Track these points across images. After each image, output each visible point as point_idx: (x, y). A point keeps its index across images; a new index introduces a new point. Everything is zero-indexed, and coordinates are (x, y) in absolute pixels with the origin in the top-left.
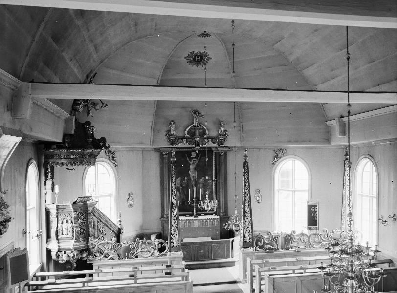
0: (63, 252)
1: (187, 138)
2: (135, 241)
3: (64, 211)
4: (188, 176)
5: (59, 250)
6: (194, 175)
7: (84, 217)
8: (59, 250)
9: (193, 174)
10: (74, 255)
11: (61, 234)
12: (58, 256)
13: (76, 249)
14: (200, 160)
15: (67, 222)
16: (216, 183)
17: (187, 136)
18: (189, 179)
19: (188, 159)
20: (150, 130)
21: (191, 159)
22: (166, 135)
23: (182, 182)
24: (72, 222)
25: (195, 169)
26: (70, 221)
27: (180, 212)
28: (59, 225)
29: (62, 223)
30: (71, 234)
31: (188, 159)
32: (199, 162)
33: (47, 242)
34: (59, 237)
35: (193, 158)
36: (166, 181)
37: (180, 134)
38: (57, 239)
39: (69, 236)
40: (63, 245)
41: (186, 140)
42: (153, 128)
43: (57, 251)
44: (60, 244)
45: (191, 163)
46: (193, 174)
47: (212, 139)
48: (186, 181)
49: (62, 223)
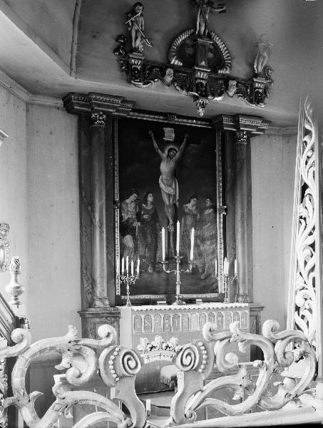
4: (157, 191)
6: (170, 191)
9: (168, 188)
16: (224, 216)
17: (175, 62)
18: (159, 201)
19: (156, 145)
21: (163, 144)
22: (116, 50)
23: (141, 208)
25: (176, 174)
27: (180, 146)
31: (156, 145)
32: (183, 155)
35: (168, 143)
36: (101, 199)
37: (156, 55)
41: (235, 83)
42: (77, 19)
45: (164, 155)
46: (168, 188)
47: (238, 83)
48: (149, 207)
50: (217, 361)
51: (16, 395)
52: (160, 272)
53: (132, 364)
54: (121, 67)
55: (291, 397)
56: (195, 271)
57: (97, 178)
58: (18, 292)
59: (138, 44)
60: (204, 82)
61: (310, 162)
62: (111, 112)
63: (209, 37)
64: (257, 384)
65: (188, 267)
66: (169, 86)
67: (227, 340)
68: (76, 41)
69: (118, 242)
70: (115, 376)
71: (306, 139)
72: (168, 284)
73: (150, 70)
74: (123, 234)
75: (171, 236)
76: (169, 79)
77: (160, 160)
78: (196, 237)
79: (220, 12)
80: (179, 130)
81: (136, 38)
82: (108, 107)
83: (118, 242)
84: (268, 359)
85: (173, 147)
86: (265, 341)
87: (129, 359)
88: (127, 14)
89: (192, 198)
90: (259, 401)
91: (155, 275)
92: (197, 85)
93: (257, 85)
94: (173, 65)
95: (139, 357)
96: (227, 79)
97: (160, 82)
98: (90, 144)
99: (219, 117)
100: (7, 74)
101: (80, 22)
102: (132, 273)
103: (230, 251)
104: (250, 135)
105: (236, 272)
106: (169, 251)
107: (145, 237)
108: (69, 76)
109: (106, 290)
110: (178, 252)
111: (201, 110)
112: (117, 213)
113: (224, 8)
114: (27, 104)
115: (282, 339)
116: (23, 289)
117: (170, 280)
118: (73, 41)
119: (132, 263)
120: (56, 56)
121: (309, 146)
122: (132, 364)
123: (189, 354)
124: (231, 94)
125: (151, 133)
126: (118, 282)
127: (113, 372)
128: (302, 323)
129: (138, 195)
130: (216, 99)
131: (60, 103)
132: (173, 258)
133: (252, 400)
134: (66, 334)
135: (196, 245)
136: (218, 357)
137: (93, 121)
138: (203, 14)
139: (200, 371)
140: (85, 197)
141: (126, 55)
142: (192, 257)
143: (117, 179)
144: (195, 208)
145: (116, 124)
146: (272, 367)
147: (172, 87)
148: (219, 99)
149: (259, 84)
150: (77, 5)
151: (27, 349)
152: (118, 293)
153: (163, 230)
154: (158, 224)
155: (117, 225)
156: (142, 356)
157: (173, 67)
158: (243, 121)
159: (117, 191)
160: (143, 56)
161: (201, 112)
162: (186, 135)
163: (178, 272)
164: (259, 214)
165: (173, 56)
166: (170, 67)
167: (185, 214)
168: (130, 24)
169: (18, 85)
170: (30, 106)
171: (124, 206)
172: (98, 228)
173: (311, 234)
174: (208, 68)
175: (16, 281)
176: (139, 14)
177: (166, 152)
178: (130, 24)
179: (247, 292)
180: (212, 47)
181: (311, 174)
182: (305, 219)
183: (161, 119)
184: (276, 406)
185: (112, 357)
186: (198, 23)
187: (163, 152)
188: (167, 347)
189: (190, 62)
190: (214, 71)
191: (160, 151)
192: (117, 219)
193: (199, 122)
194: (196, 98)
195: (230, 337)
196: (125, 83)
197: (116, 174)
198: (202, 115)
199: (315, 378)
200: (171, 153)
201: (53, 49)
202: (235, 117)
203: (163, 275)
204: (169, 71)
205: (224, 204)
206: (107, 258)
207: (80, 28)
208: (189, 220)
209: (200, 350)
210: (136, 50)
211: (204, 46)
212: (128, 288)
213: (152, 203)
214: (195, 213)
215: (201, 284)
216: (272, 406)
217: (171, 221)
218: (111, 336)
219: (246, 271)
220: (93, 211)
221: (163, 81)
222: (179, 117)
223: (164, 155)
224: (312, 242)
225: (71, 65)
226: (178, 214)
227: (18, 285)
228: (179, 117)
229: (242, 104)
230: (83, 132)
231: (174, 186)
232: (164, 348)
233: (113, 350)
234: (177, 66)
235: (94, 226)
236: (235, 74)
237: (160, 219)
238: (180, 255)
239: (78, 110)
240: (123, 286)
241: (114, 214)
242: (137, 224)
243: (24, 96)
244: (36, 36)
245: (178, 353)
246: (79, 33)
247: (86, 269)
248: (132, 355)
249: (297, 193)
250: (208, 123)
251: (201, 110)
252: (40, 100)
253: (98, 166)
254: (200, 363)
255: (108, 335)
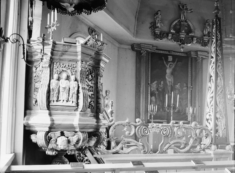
0: (58, 133)
1: (173, 34)
2: (82, 157)
3: (65, 57)
4: (164, 79)
5: (50, 128)
7: (92, 76)
8: (51, 128)
10: (78, 142)
11: (55, 99)
12: (48, 140)
13: (82, 128)
14: (176, 65)
15: (68, 78)
17: (172, 31)
18: (165, 84)
19: (165, 63)
20: (134, 19)
21: (168, 62)
22: (151, 27)
23: (158, 86)
24: (76, 80)
25: (172, 74)
26: (73, 78)
28: (54, 82)
29: (59, 79)
30: (75, 100)
31: (165, 63)
33: (25, 115)
34: (52, 103)
35: (170, 62)
36: (143, 83)
37: (165, 29)
38: (48, 107)
39: (70, 104)
40: (60, 119)
41: (196, 39)
42: (137, 17)
43: (47, 130)
44: (54, 117)
45: (168, 66)
46: (169, 79)
47: (197, 38)
48: (162, 86)
49: (59, 79)
50: (175, 134)
51: (110, 138)
52: (165, 111)
53: (146, 132)
54: (152, 34)
55: (202, 149)
56: (179, 111)
57: (142, 74)
58: (112, 113)
59: (159, 25)
60: (183, 38)
61: (213, 68)
62: (148, 50)
63: (186, 21)
64: (189, 143)
65: (176, 110)
66: (170, 40)
67: (178, 127)
68: (136, 24)
69: (149, 99)
70: (140, 135)
71: (212, 59)
72: (168, 116)
73: (163, 34)
74: (151, 96)
75: (170, 98)
76: (170, 38)
77: (166, 68)
78: (180, 98)
79: (191, 12)
80: (174, 57)
81: (158, 23)
82: (147, 48)
83: (149, 99)
84: (194, 135)
85: (172, 63)
86: (193, 129)
87: (145, 130)
88: (155, 14)
89: (178, 83)
90: (190, 149)
91: (163, 113)
92: (181, 40)
93: (205, 39)
94: (172, 32)
95: (149, 130)
96: (193, 37)
97: (166, 39)
98: (140, 62)
99: (190, 52)
100: (113, 39)
101: (138, 18)
102: (154, 111)
103: (193, 105)
104: (203, 59)
105: (195, 112)
106: (169, 103)
107: (159, 97)
108: (133, 37)
109: (144, 117)
110: (172, 103)
111: (182, 49)
112: (149, 88)
113: (192, 11)
114: (118, 48)
115: (199, 129)
116: (114, 111)
117: (169, 115)
118: (135, 25)
119: (154, 107)
120: (129, 31)
121: (212, 62)
122: (146, 132)
123: (165, 131)
124: (194, 43)
125: (163, 58)
126: (149, 114)
127: (140, 134)
128: (208, 124)
129: (157, 81)
130: (188, 45)
131: (130, 47)
132: (170, 106)
133: (187, 148)
134: (126, 120)
135: (180, 102)
136: (175, 133)
137: (141, 54)
138: (183, 13)
139: (169, 136)
140: (138, 82)
141: (154, 29)
142: (177, 106)
143: (150, 75)
144: (179, 87)
145: (150, 54)
146: (195, 138)
147: (171, 40)
148: (190, 45)
149: (206, 39)
150: (137, 12)
151: (114, 124)
152: (149, 118)
153: (167, 95)
154: (165, 93)
155: (149, 92)
156: (149, 129)
157: (171, 33)
158: (199, 53)
159: (149, 80)
160: (160, 29)
161: (182, 50)
162: (177, 59)
163: (172, 111)
164: (127, 58)
165: (172, 29)
166: (171, 33)
167: (175, 89)
168: (156, 18)
169: (116, 41)
170: (119, 49)
171: (152, 86)
172: (142, 93)
173: (212, 93)
174: (185, 33)
175: (112, 109)
176: (159, 14)
177: (169, 65)
178: (156, 18)
179: (199, 121)
180: (187, 25)
181: (213, 72)
182: (211, 88)
183: (167, 53)
184: (196, 152)
185: (140, 129)
186: (181, 16)
187: (167, 65)
188: (158, 127)
189: (178, 31)
190: (188, 34)
191: (166, 65)
192: (149, 90)
193: (182, 54)
194: (180, 45)
195: (180, 126)
196: (154, 40)
197: (150, 73)
198: (182, 51)
199: (211, 144)
200: (171, 66)
201: (128, 28)
202: (196, 52)
203: (166, 112)
204: (170, 35)
205: (191, 86)
206: (145, 105)
207: (137, 20)
208: (177, 92)
209: (169, 129)
210: (158, 27)
211: (183, 25)
212: (152, 117)
213: (163, 85)
214: (179, 88)
215: (181, 116)
216: (194, 151)
217: (170, 92)
218: (140, 122)
219: (200, 112)
220: (140, 87)
221: (168, 38)
222: (174, 52)
223: (168, 66)
224: (212, 96)
225: (134, 33)
226: (173, 89)
227: (112, 110)
228: (174, 52)
229: (199, 47)
230: (138, 58)
231: (171, 78)
232: (157, 128)
233: (141, 127)
234: (173, 33)
235: (141, 93)
236: (196, 35)
237: (166, 91)
238: (173, 105)
239: (136, 50)
240: (151, 116)
241: (148, 88)
242: (157, 92)
243: (117, 45)
244: (122, 24)
245: (162, 130)
246: (137, 22)
247: (137, 108)
248: (146, 129)
249: (208, 79)
250: (185, 54)
251: (182, 49)
252: (123, 46)
253: (143, 70)
254: (169, 134)
255: (139, 122)
